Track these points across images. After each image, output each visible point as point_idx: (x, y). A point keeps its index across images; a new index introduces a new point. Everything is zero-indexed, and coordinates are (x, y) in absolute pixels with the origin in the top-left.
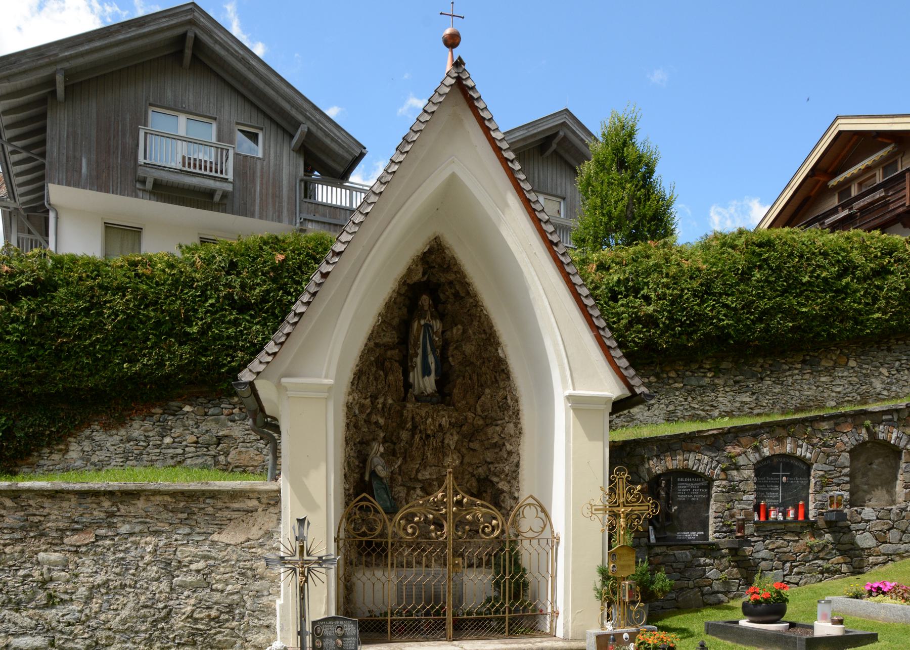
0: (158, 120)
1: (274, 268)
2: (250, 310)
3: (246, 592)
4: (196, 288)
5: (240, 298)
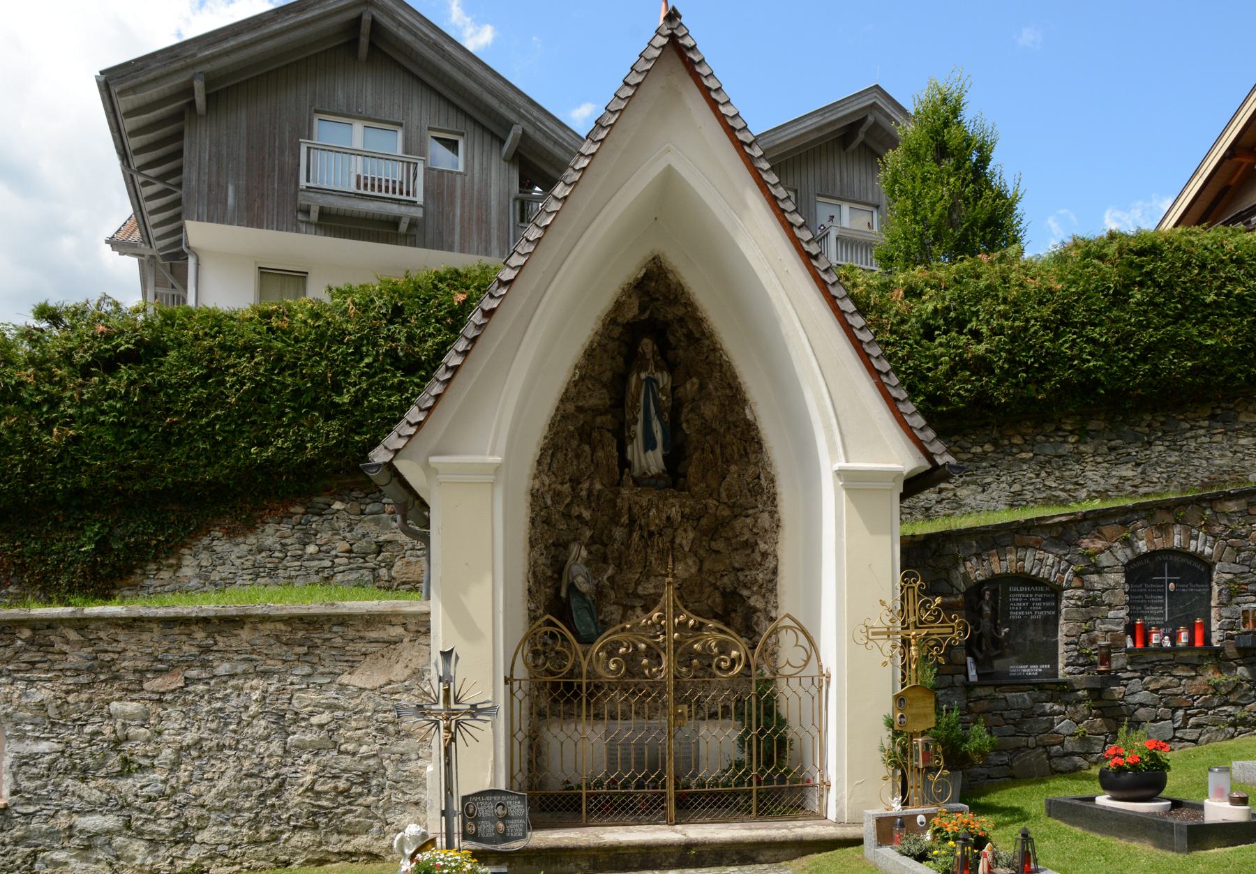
0: (327, 131)
1: (452, 313)
2: (421, 369)
3: (386, 755)
4: (347, 344)
5: (406, 355)
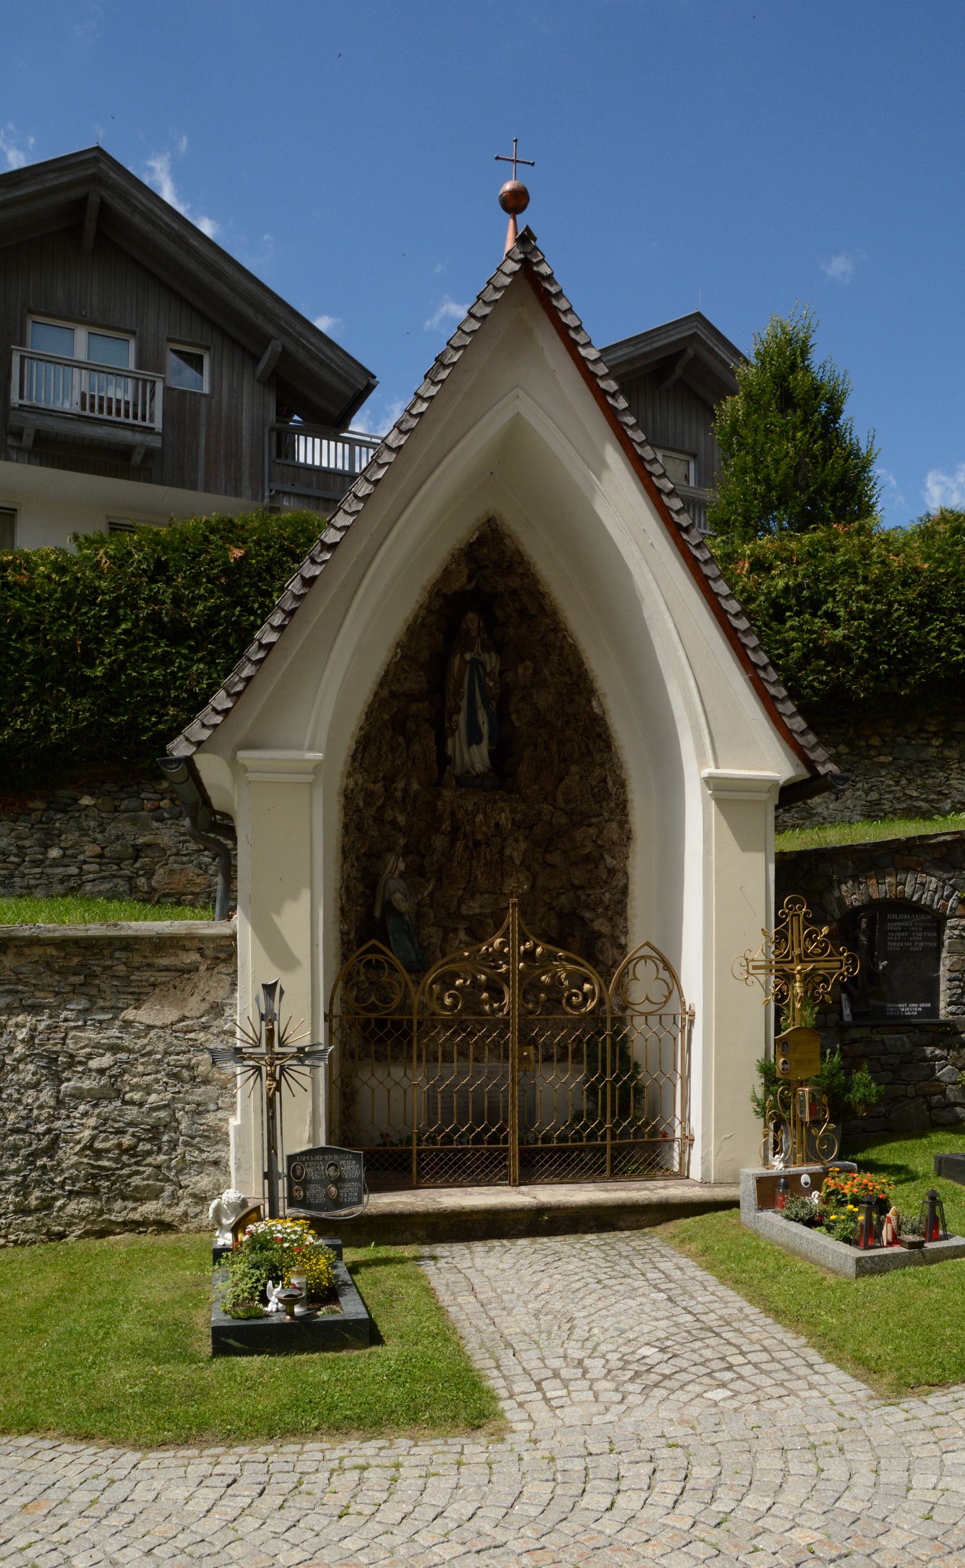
0: (43, 337)
3: (180, 1106)
4: (100, 605)
5: (172, 620)
